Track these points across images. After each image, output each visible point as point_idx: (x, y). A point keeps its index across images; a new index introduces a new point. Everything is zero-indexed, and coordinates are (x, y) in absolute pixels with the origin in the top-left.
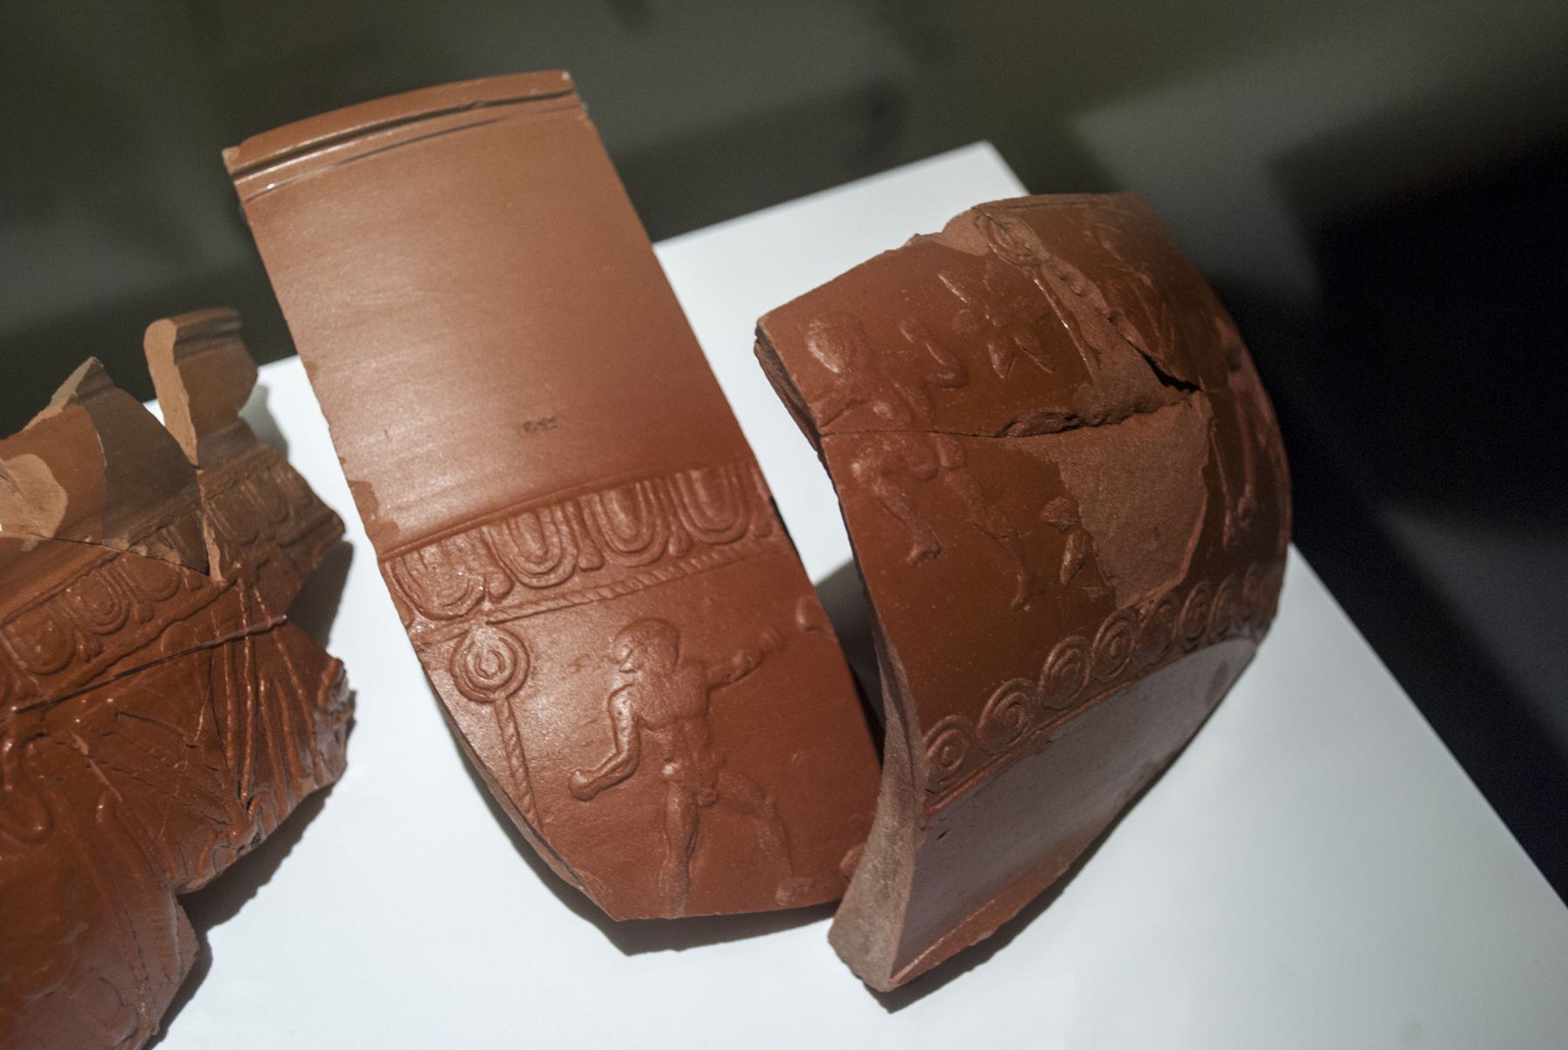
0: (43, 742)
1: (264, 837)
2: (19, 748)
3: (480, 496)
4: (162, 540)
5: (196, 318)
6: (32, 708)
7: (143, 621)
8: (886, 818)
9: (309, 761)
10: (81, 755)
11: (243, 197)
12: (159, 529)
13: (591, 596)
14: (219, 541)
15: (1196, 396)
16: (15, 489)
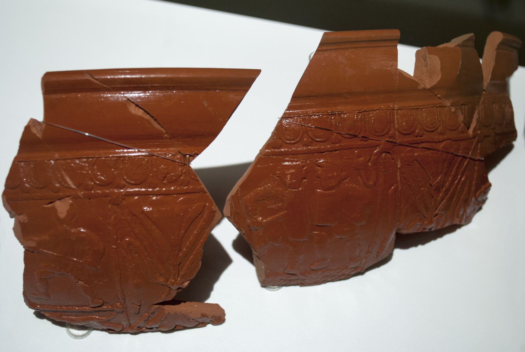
0: (389, 155)
1: (433, 229)
5: (510, 37)
6: (391, 142)
7: (441, 134)
9: (461, 213)
10: (397, 167)
12: (462, 105)
14: (478, 120)
16: (426, 66)
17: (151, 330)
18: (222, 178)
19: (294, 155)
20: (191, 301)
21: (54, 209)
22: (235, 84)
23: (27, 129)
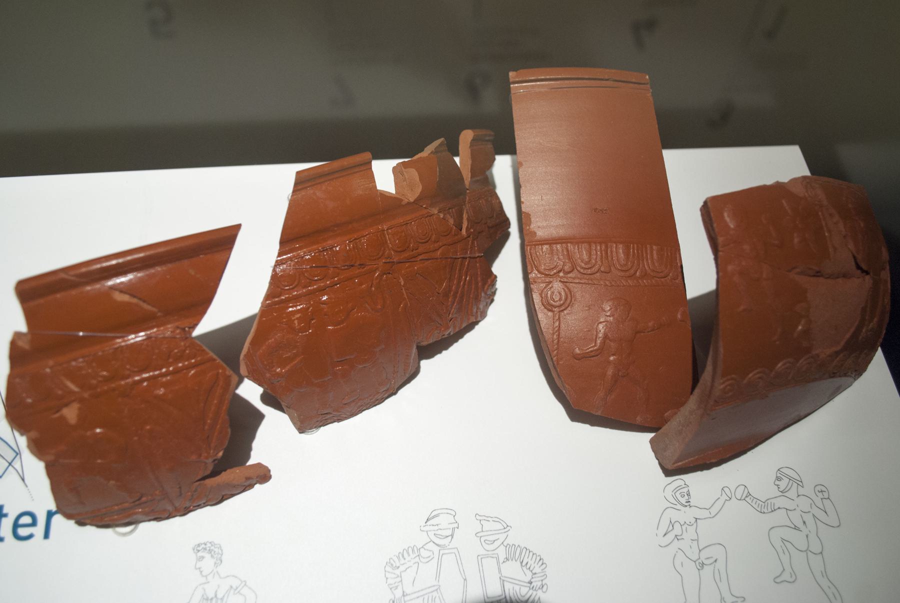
2: (381, 276)
3: (562, 232)
4: (449, 213)
5: (480, 132)
8: (692, 403)
9: (475, 310)
11: (512, 92)
13: (602, 283)
14: (468, 220)
15: (867, 277)
17: (199, 507)
18: (230, 338)
19: (296, 300)
20: (231, 467)
21: (63, 418)
22: (217, 245)
23: (13, 345)
